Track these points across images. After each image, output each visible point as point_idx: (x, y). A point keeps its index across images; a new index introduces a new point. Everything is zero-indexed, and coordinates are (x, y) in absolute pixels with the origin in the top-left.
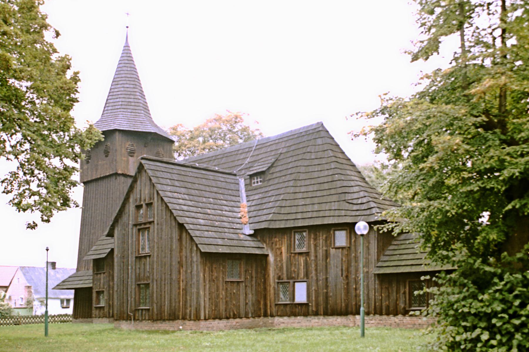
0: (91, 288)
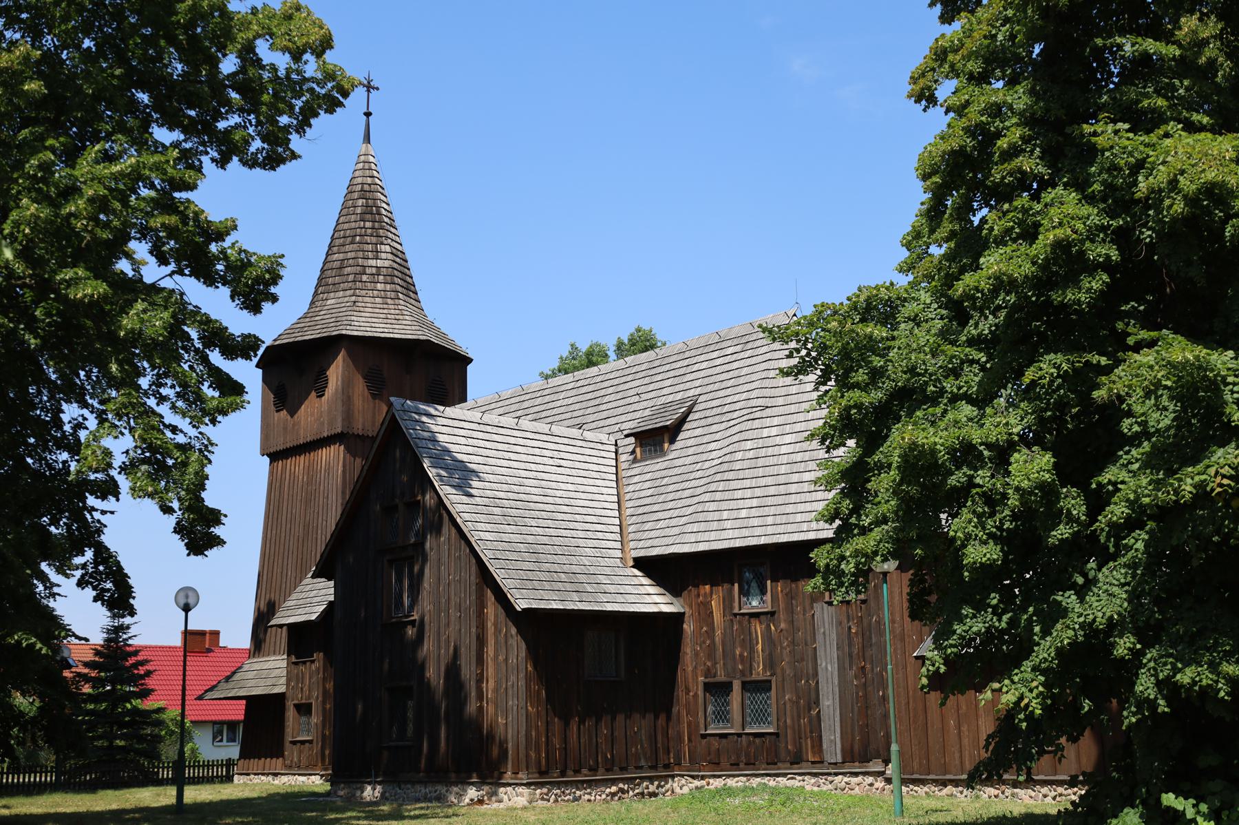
0: (281, 696)
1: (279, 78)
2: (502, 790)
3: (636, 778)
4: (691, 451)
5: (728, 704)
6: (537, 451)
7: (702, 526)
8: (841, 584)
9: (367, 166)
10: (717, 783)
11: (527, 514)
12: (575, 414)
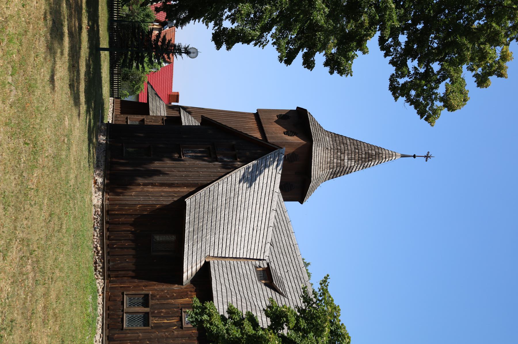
1: (432, 90)
2: (101, 193)
3: (104, 260)
4: (261, 292)
5: (138, 306)
6: (260, 219)
7: (225, 294)
8: (196, 314)
9: (391, 155)
10: (100, 299)
11: (231, 210)
12: (278, 244)
